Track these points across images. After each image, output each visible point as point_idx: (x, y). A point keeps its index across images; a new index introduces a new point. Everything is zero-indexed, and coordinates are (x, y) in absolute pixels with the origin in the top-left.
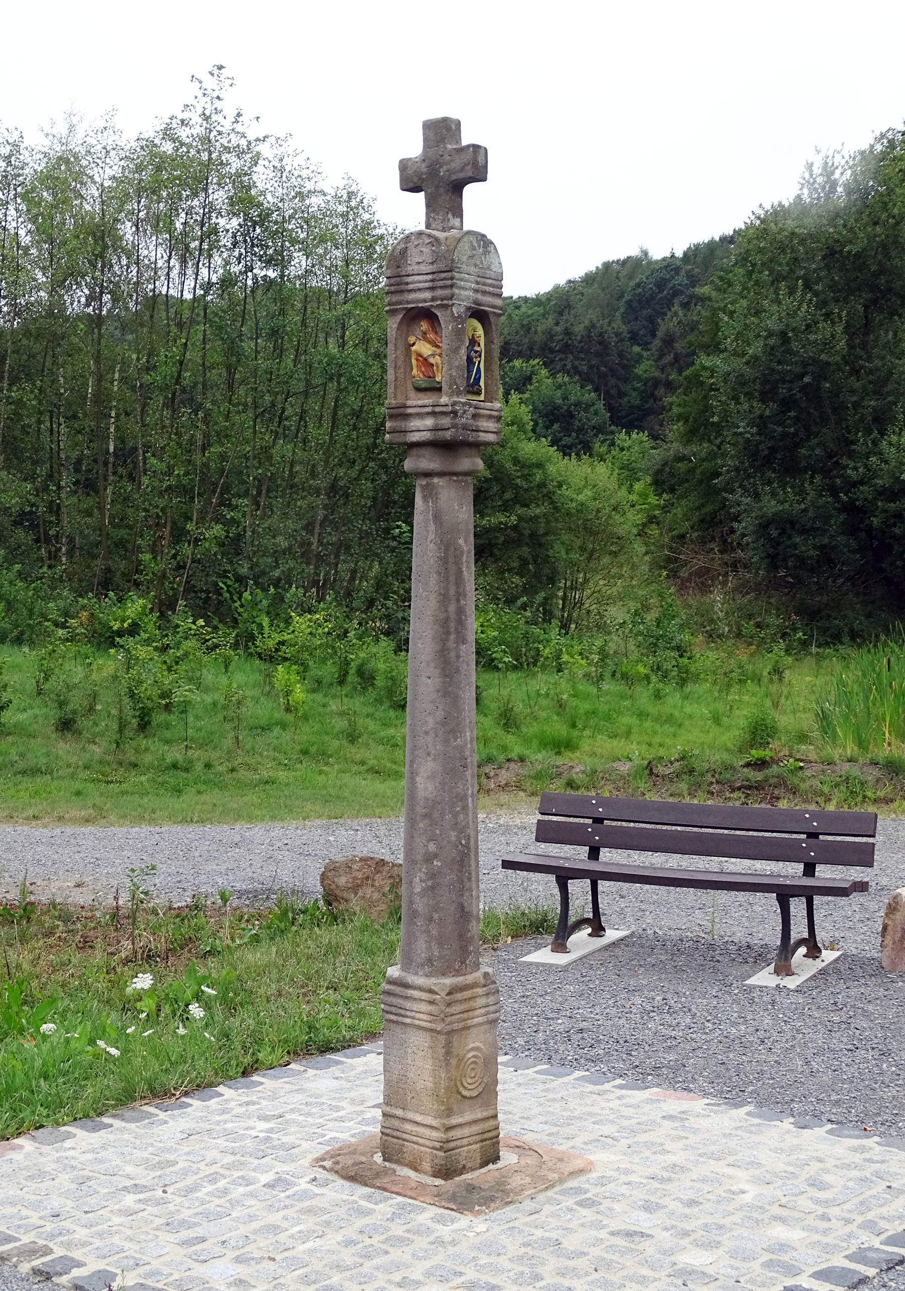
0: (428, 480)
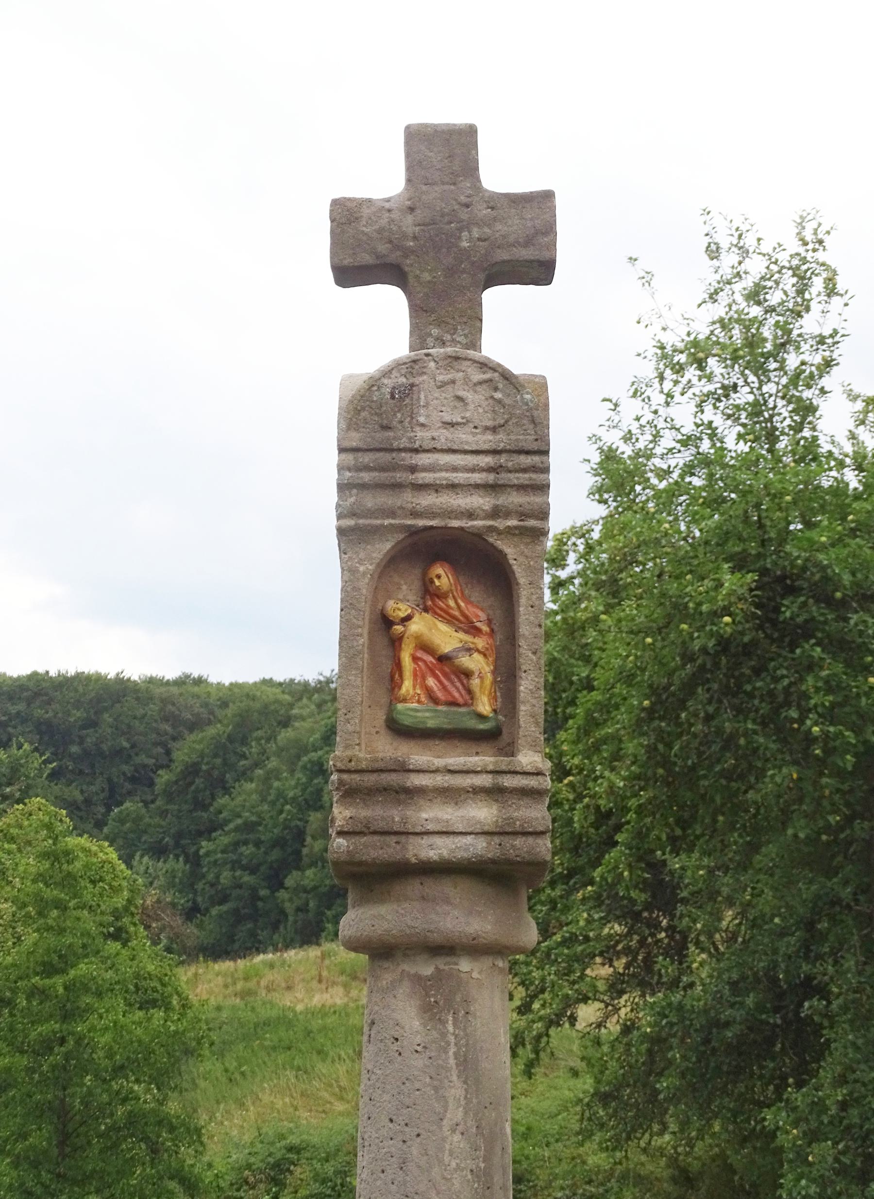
0: (441, 963)
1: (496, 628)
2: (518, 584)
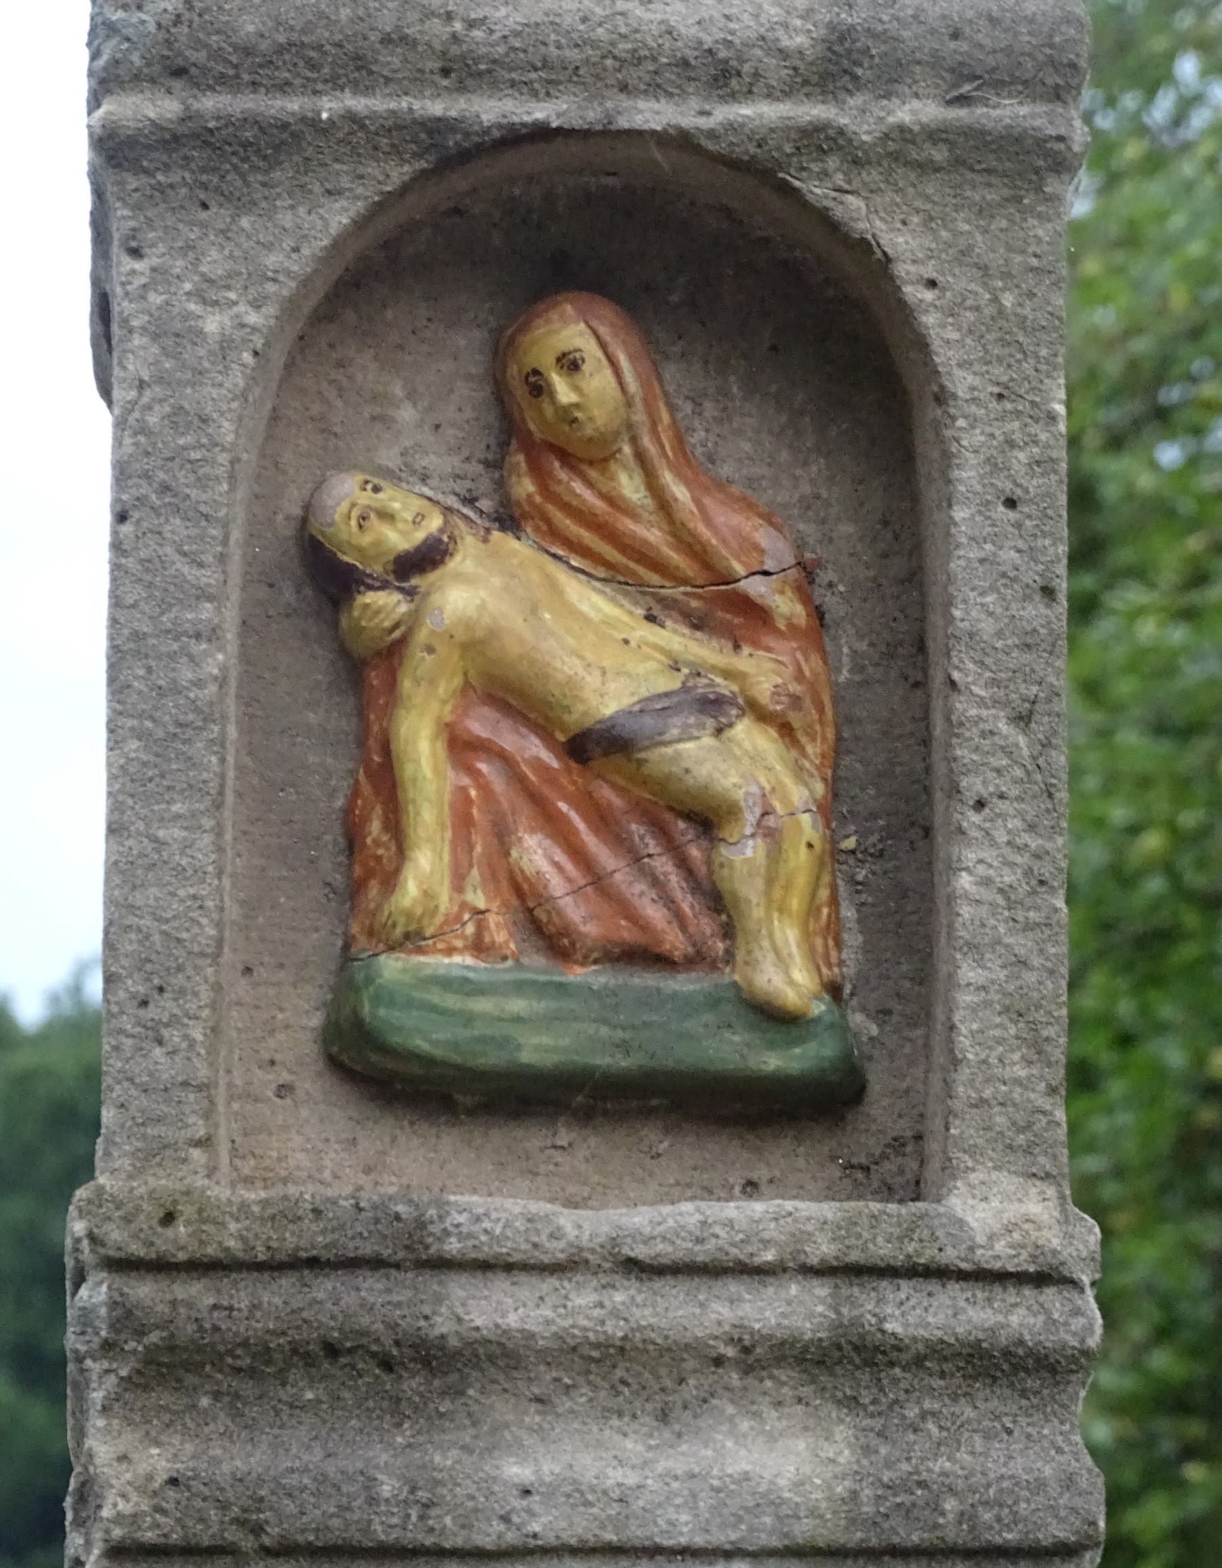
1: (833, 605)
2: (942, 397)
